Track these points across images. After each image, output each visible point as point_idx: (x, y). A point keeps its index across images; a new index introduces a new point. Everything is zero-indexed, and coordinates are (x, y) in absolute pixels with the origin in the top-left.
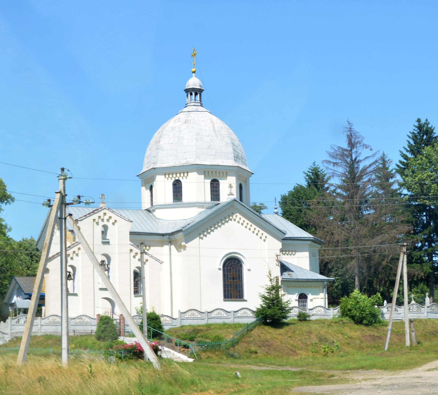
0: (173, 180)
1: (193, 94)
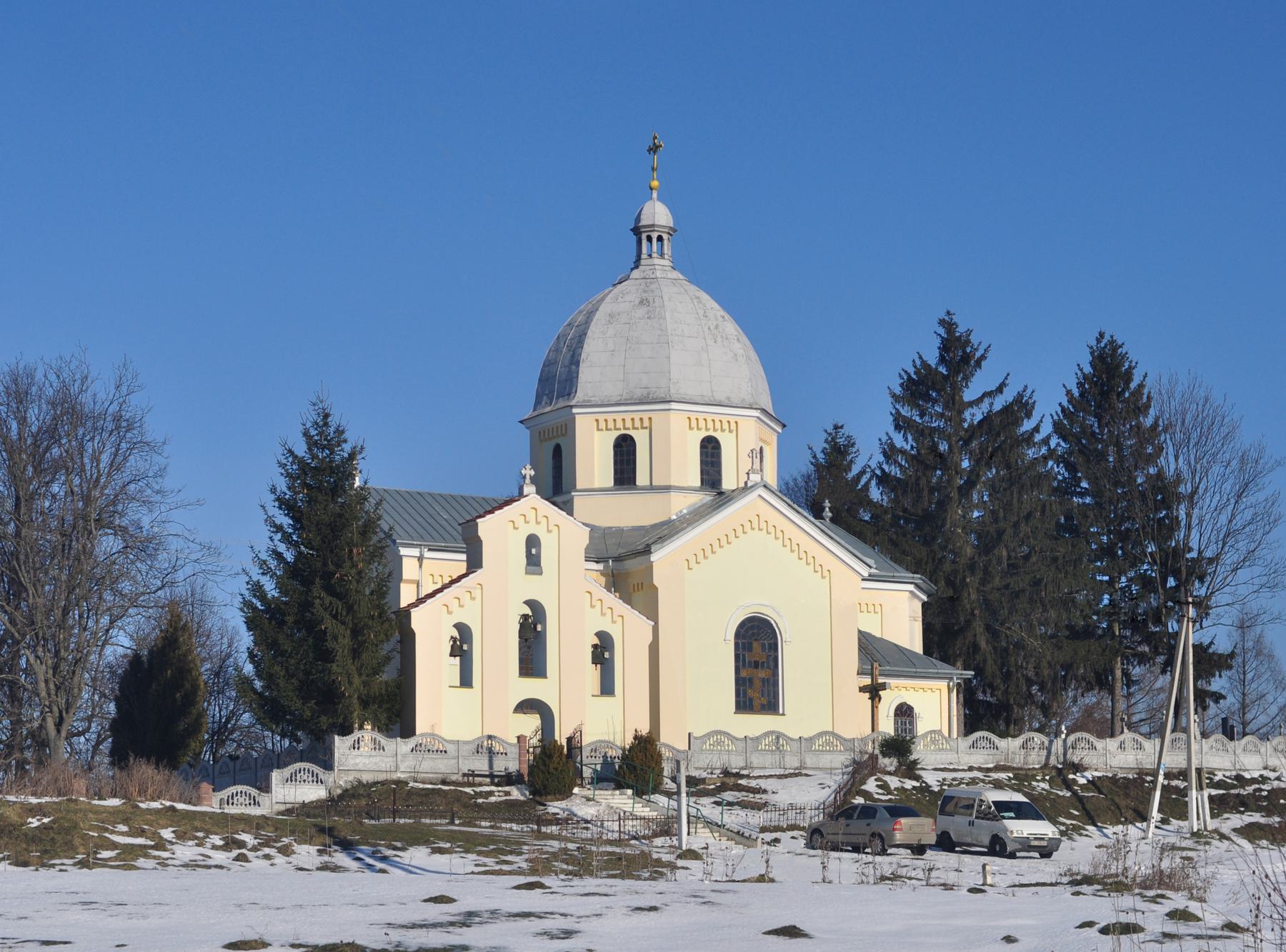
0: (617, 434)
1: (654, 240)
